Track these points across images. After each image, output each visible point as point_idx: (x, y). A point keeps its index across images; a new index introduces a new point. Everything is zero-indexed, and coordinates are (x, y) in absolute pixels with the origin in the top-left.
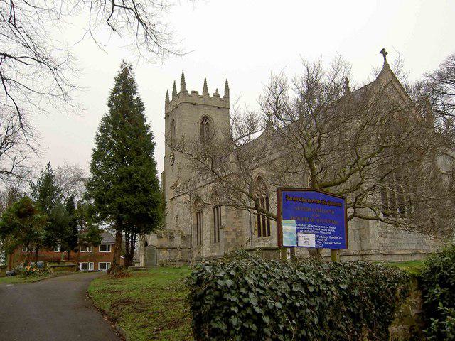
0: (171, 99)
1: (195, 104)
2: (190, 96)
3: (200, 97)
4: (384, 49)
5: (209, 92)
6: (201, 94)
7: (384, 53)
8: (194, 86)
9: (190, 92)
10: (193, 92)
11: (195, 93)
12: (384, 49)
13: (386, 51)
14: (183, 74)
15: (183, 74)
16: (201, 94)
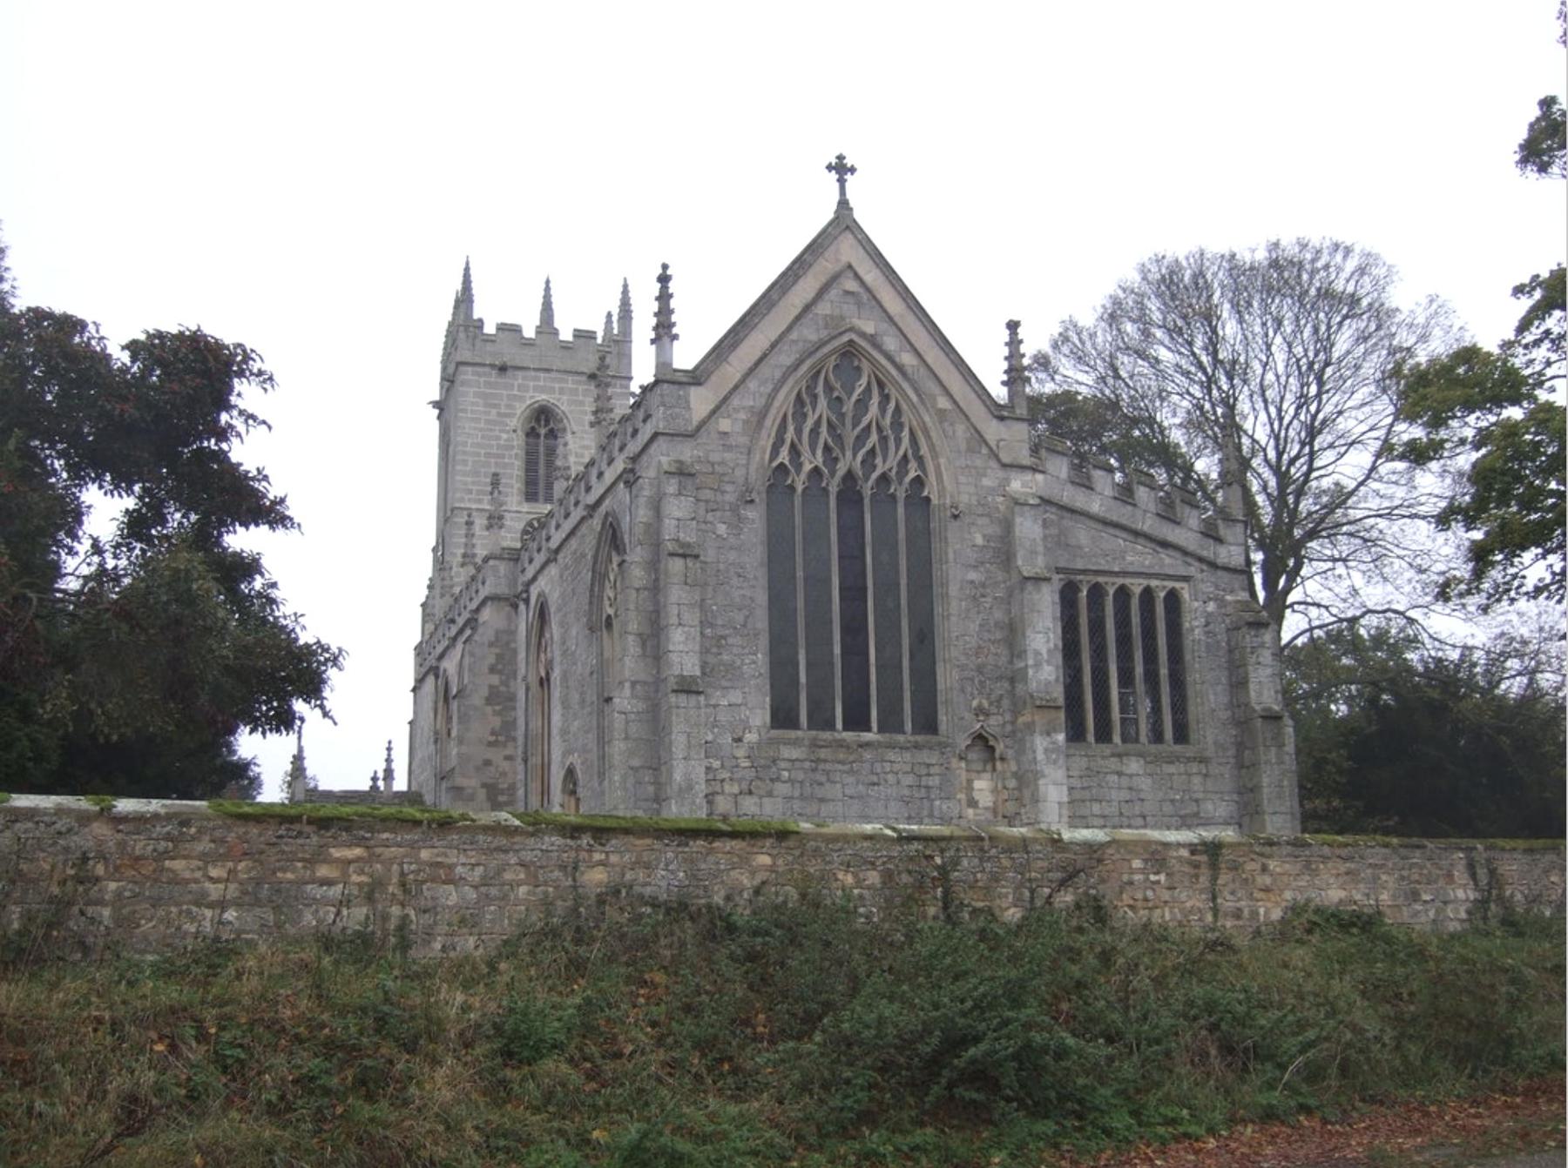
0: (244, 936)
1: (503, 369)
2: (489, 339)
3: (529, 343)
4: (841, 158)
5: (557, 324)
6: (529, 332)
7: (841, 168)
8: (246, 394)
9: (489, 329)
10: (502, 328)
11: (510, 330)
12: (841, 158)
13: (849, 162)
14: (467, 269)
15: (467, 269)
16: (529, 332)
